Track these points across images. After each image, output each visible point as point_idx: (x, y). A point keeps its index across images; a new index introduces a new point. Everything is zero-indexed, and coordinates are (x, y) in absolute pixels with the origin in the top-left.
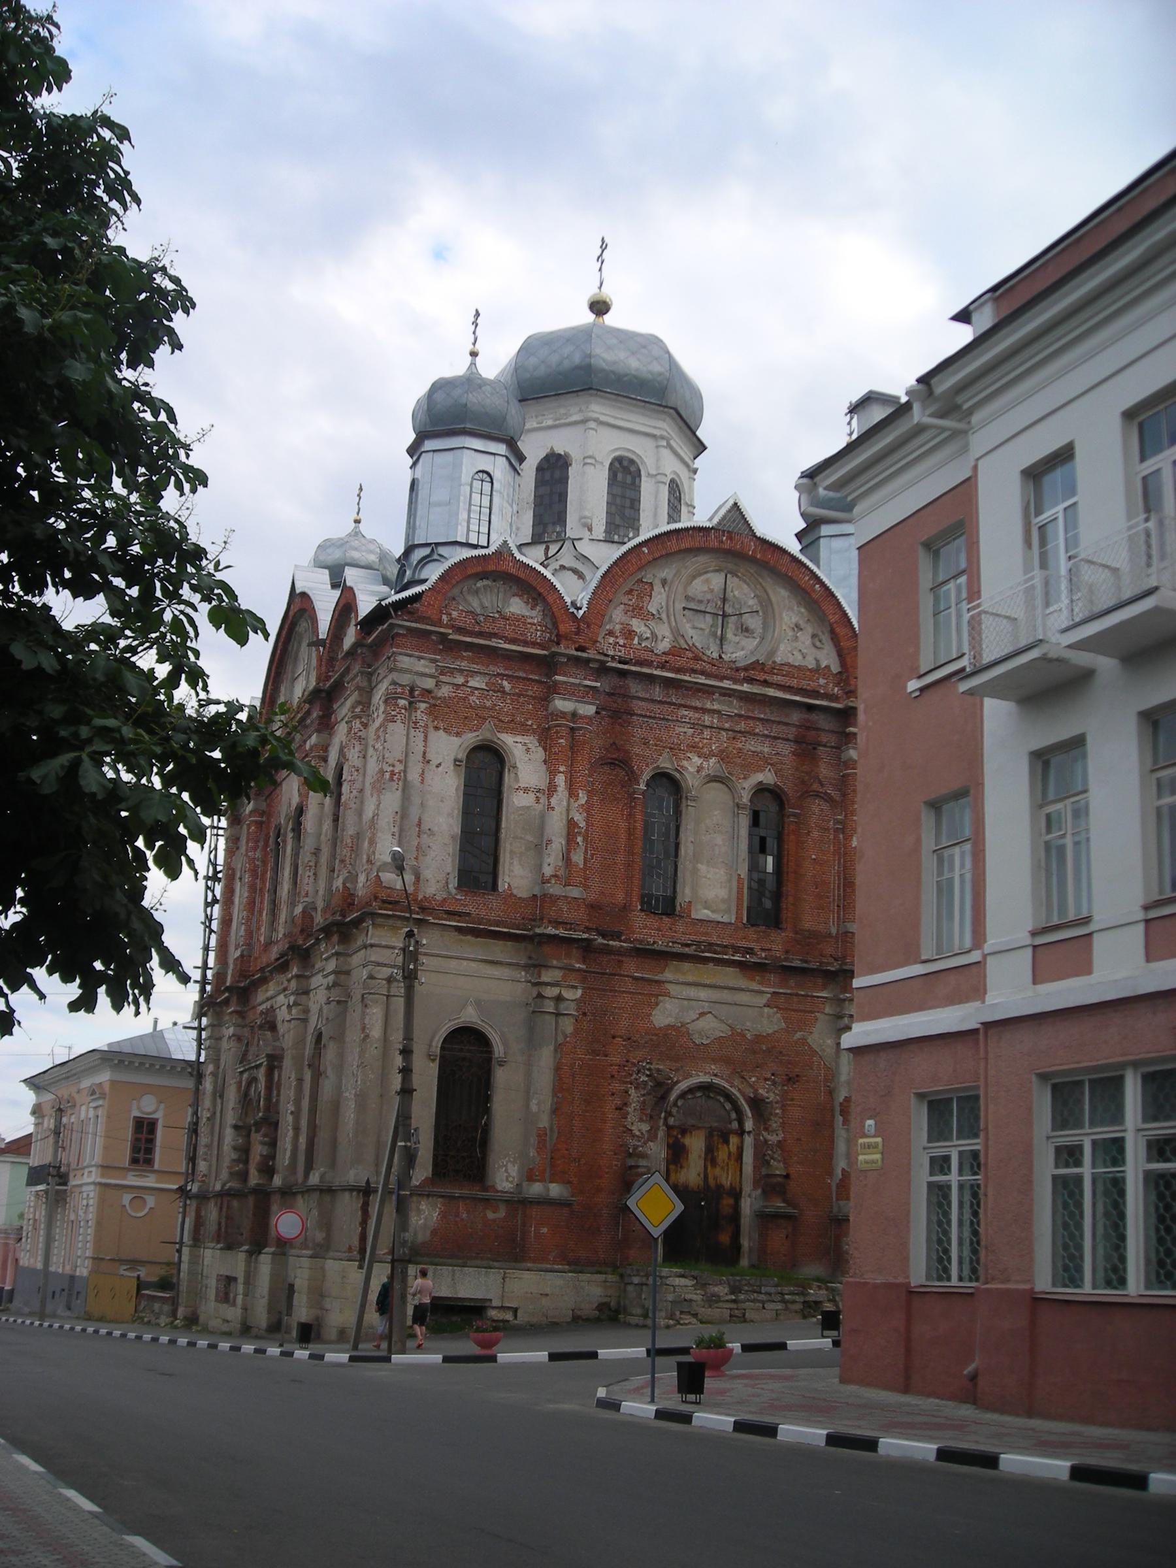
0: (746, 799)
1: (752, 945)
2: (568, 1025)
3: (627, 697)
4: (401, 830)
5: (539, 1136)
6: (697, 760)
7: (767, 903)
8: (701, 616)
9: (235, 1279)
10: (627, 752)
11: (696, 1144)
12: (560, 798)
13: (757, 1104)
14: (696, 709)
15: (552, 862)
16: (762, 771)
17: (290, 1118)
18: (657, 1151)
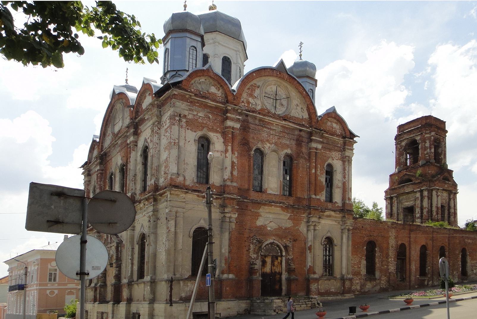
0: (282, 159)
2: (233, 226)
3: (248, 122)
4: (178, 162)
5: (225, 260)
6: (268, 145)
7: (290, 187)
9: (107, 313)
10: (248, 141)
11: (269, 260)
12: (229, 154)
13: (286, 247)
14: (268, 128)
15: (227, 175)
17: (130, 261)
18: (259, 263)
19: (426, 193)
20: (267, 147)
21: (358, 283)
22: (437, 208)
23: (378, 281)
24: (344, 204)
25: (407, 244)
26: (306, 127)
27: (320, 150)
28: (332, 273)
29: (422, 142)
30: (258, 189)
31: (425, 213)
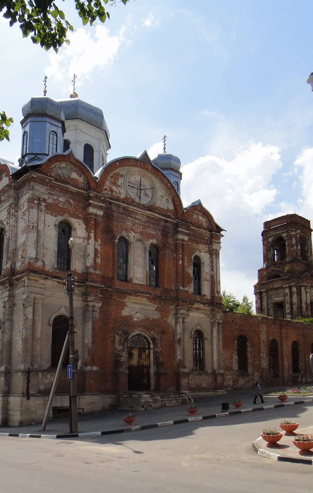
0: (148, 248)
1: (151, 292)
2: (97, 315)
3: (111, 210)
4: (37, 247)
7: (156, 277)
8: (133, 189)
10: (112, 229)
11: (135, 352)
12: (92, 241)
13: (154, 339)
14: (133, 217)
15: (90, 262)
16: (153, 239)
18: (125, 355)
19: (294, 289)
20: (132, 236)
21: (230, 379)
22: (306, 303)
23: (251, 377)
24: (213, 296)
25: (278, 340)
26: (171, 218)
27: (187, 242)
28: (203, 368)
29: (288, 240)
30: (123, 278)
31: (295, 309)
